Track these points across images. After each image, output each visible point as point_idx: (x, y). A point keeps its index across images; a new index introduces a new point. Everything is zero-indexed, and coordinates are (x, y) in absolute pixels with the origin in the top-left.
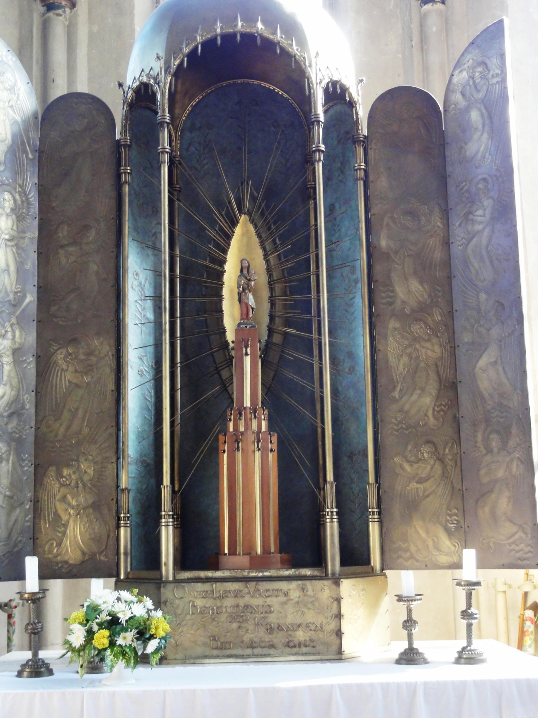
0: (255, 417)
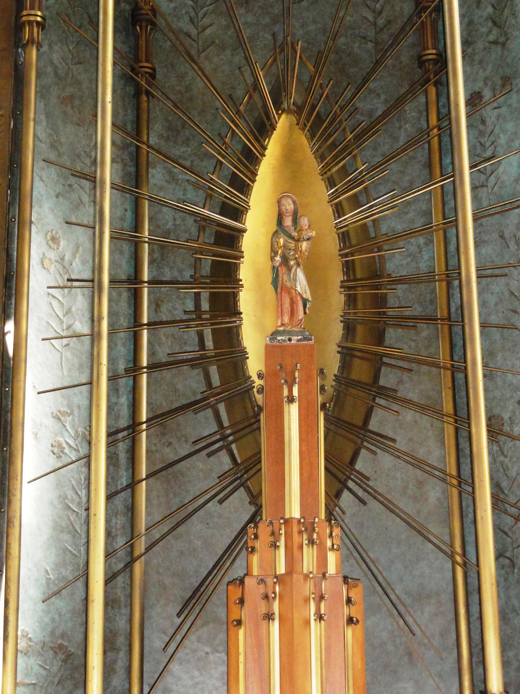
0: (312, 542)
